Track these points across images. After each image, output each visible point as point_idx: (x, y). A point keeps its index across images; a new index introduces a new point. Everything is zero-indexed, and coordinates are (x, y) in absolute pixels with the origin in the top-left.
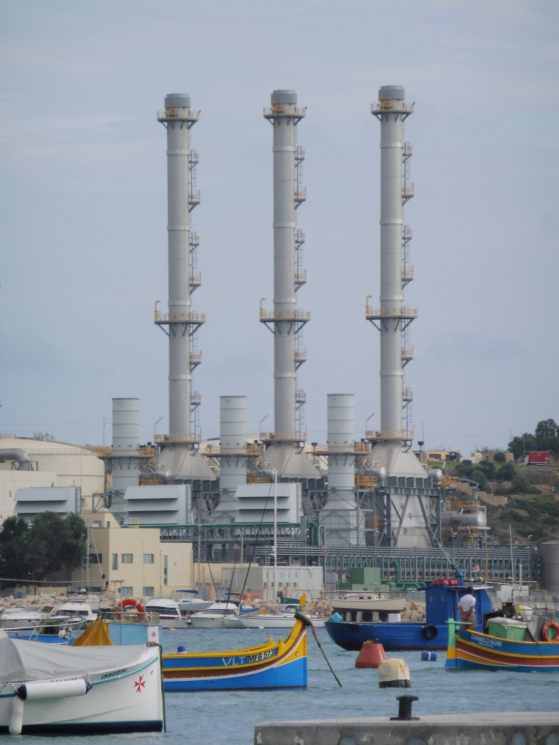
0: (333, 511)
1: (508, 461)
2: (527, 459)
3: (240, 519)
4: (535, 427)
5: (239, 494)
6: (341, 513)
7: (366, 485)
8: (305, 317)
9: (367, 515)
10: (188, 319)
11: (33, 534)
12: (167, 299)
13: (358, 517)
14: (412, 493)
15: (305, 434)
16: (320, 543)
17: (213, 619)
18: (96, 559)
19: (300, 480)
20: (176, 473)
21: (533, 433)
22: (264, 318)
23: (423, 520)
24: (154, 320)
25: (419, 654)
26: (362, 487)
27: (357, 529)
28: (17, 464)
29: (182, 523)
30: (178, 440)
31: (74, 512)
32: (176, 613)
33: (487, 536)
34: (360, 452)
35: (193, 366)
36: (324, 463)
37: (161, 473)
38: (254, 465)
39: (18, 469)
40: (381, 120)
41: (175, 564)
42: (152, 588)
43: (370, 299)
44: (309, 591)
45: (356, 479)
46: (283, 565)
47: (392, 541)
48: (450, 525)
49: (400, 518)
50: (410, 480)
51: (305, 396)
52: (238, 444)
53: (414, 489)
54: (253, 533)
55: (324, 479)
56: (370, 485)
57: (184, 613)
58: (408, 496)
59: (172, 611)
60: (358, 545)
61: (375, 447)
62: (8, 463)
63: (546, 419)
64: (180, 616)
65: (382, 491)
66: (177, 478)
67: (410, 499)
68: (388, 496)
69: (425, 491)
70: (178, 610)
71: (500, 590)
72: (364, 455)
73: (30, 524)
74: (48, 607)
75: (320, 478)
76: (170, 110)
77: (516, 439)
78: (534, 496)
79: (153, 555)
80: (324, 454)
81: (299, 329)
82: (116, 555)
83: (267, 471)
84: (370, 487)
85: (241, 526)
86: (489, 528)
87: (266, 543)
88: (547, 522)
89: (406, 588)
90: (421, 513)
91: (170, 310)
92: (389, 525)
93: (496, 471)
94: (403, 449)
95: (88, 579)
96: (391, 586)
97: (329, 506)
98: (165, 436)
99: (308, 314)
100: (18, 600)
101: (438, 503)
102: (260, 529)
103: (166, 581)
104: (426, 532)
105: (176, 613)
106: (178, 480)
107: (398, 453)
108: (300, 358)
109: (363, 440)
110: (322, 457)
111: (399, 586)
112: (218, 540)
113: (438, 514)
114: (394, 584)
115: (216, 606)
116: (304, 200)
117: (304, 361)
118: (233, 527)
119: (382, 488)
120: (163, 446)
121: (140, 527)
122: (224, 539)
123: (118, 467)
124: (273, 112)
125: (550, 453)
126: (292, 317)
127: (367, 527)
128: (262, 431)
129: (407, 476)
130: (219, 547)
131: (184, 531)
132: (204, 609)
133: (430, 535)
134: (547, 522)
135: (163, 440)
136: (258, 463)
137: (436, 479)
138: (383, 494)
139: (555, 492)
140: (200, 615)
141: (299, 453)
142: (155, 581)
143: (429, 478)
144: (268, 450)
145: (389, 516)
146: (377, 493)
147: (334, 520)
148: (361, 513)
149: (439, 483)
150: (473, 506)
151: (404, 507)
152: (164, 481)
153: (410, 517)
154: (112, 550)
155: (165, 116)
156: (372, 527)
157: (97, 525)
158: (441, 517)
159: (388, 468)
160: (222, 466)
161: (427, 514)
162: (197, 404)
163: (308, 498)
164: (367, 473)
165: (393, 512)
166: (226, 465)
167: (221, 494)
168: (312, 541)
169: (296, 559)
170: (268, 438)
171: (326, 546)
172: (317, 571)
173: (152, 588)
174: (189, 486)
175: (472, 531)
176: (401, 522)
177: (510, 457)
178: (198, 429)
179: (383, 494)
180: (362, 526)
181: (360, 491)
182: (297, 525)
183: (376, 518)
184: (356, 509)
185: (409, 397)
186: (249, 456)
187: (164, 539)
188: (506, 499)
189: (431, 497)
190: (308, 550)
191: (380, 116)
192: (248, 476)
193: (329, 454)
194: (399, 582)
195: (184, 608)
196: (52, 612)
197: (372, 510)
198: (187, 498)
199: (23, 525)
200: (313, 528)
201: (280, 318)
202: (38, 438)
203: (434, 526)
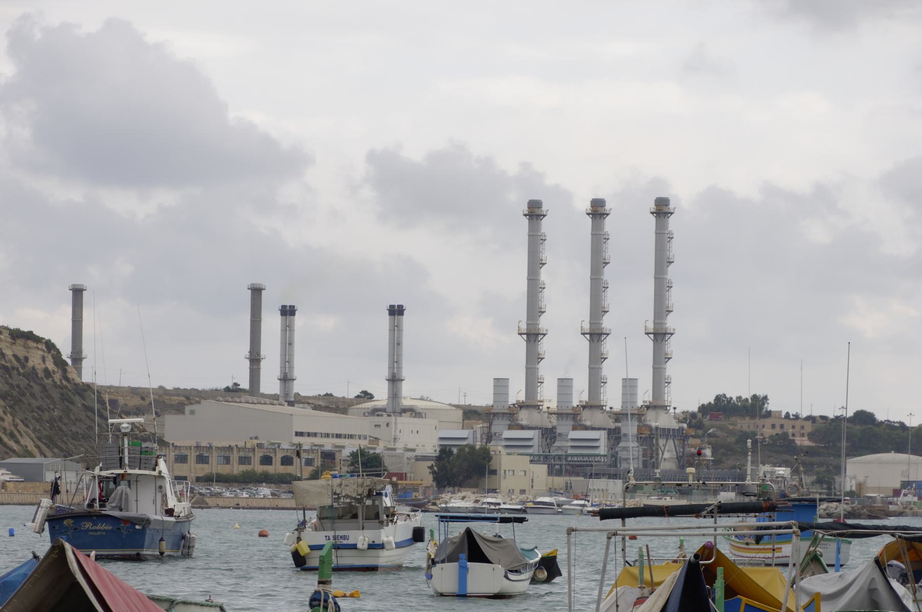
1: (698, 418)
3: (570, 452)
7: (644, 432)
8: (672, 332)
9: (644, 450)
10: (537, 332)
13: (639, 451)
14: (669, 437)
15: (670, 402)
17: (575, 509)
18: (494, 472)
19: (540, 428)
20: (592, 424)
22: (582, 332)
23: (675, 453)
25: (376, 543)
26: (641, 434)
27: (638, 458)
29: (602, 453)
30: (593, 404)
32: (554, 506)
33: (711, 463)
34: (640, 413)
35: (539, 360)
36: (554, 419)
37: (521, 423)
38: (576, 420)
40: (656, 217)
41: (538, 477)
42: (525, 491)
43: (583, 323)
45: (638, 429)
46: (598, 478)
48: (690, 457)
49: (662, 452)
50: (669, 429)
51: (607, 379)
52: (568, 407)
53: (671, 435)
54: (590, 460)
55: (554, 428)
56: (646, 432)
58: (667, 440)
60: (638, 467)
61: (649, 410)
62: (409, 413)
63: (721, 394)
64: (556, 507)
65: (652, 436)
66: (593, 427)
67: (669, 440)
69: (677, 437)
70: (555, 504)
71: (719, 494)
72: (578, 414)
73: (455, 451)
74: (477, 500)
75: (551, 427)
76: (531, 209)
77: (703, 405)
78: (715, 439)
79: (513, 471)
80: (555, 414)
81: (604, 339)
82: (505, 471)
84: (646, 434)
85: (572, 456)
86: (712, 459)
87: (588, 466)
89: (666, 493)
90: (674, 450)
91: (527, 327)
93: (693, 424)
94: (666, 412)
95: (749, 478)
98: (586, 402)
100: (453, 495)
102: (589, 458)
104: (676, 460)
105: (554, 506)
106: (530, 427)
107: (662, 414)
108: (669, 356)
109: (578, 406)
110: (554, 415)
112: (558, 463)
114: (659, 490)
116: (609, 263)
117: (544, 358)
118: (567, 456)
121: (518, 455)
124: (529, 212)
125: (722, 414)
127: (643, 457)
128: (581, 400)
129: (667, 428)
131: (538, 457)
132: (569, 503)
135: (584, 404)
136: (578, 419)
139: (727, 437)
140: (566, 507)
143: (679, 429)
144: (584, 411)
148: (640, 449)
149: (684, 432)
150: (704, 445)
151: (665, 446)
152: (523, 428)
153: (668, 451)
154: (503, 467)
155: (527, 213)
157: (494, 453)
161: (678, 450)
162: (669, 383)
163: (544, 440)
164: (644, 425)
166: (560, 419)
167: (557, 436)
168: (614, 465)
169: (603, 475)
170: (648, 404)
173: (525, 491)
174: (540, 431)
175: (703, 460)
176: (663, 454)
177: (700, 415)
178: (669, 397)
180: (641, 457)
181: (640, 436)
182: (604, 456)
183: (649, 452)
184: (638, 447)
187: (531, 461)
188: (700, 440)
189: (680, 440)
190: (612, 470)
191: (655, 215)
193: (557, 414)
194: (663, 490)
195: (558, 503)
196: (480, 503)
198: (539, 438)
199: (451, 452)
200: (614, 456)
201: (593, 332)
203: (681, 457)
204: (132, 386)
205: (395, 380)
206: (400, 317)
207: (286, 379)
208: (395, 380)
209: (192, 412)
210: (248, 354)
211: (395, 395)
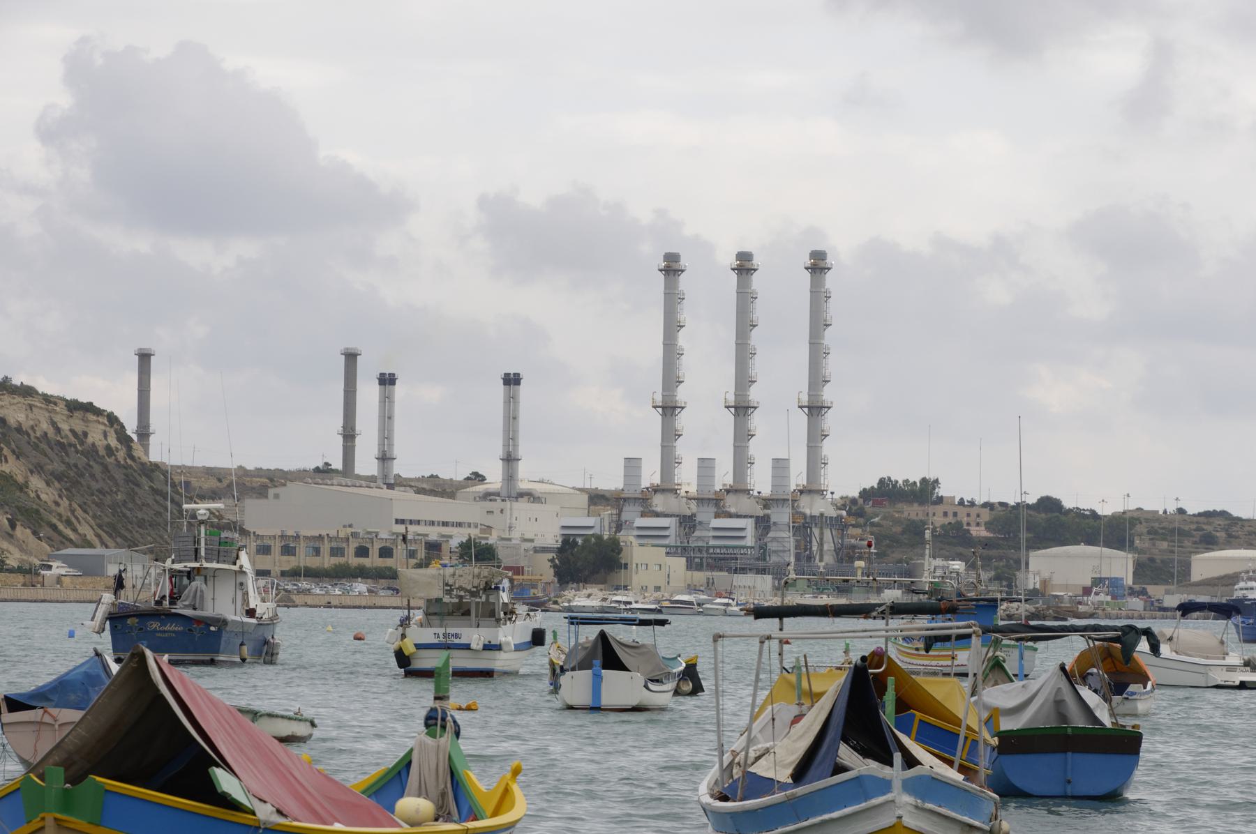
0: (774, 538)
2: (871, 503)
3: (712, 542)
4: (877, 481)
5: (712, 525)
6: (780, 540)
9: (797, 541)
10: (747, 405)
11: (583, 547)
12: (807, 391)
16: (768, 559)
17: (717, 609)
19: (677, 516)
21: (876, 486)
24: (724, 405)
28: (532, 499)
29: (749, 544)
31: (599, 533)
32: (694, 605)
37: (654, 509)
38: (719, 506)
39: (533, 502)
44: (763, 591)
47: (813, 559)
55: (694, 515)
57: (699, 605)
59: (691, 603)
62: (526, 498)
64: (696, 606)
65: (807, 525)
68: (811, 529)
73: (580, 541)
77: (865, 489)
78: (878, 528)
80: (694, 499)
83: (728, 510)
85: (714, 547)
88: (888, 546)
92: (811, 548)
93: (853, 511)
96: (813, 589)
97: (771, 534)
99: (832, 403)
101: (843, 534)
103: (668, 582)
104: (834, 553)
105: (694, 605)
111: (818, 589)
112: (698, 556)
113: (842, 541)
115: (718, 600)
119: (807, 523)
120: (655, 491)
122: (702, 556)
123: (775, 505)
126: (820, 404)
127: (796, 549)
130: (697, 560)
132: (711, 602)
133: (837, 555)
134: (888, 546)
137: (842, 517)
138: (808, 527)
140: (708, 606)
141: (823, 499)
142: (662, 583)
143: (838, 516)
145: (811, 542)
146: (804, 527)
147: (775, 544)
154: (634, 562)
156: (800, 549)
158: (845, 543)
159: (811, 509)
160: (698, 506)
163: (682, 529)
164: (797, 513)
165: (814, 538)
166: (701, 505)
170: (728, 487)
171: (771, 562)
172: (768, 578)
174: (753, 519)
177: (861, 501)
179: (808, 527)
185: (826, 462)
186: (717, 500)
190: (761, 564)
192: (716, 513)
195: (699, 602)
197: (799, 538)
199: (575, 543)
200: (763, 548)
202: (542, 482)
203: (840, 549)
204: (286, 469)
205: (510, 460)
206: (516, 387)
207: (385, 458)
208: (510, 460)
209: (277, 496)
210: (341, 429)
211: (510, 477)
